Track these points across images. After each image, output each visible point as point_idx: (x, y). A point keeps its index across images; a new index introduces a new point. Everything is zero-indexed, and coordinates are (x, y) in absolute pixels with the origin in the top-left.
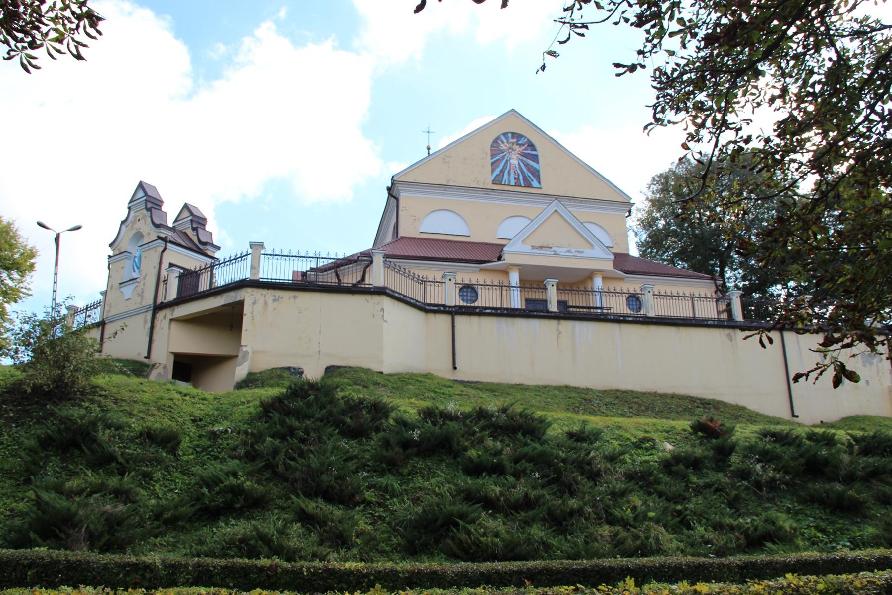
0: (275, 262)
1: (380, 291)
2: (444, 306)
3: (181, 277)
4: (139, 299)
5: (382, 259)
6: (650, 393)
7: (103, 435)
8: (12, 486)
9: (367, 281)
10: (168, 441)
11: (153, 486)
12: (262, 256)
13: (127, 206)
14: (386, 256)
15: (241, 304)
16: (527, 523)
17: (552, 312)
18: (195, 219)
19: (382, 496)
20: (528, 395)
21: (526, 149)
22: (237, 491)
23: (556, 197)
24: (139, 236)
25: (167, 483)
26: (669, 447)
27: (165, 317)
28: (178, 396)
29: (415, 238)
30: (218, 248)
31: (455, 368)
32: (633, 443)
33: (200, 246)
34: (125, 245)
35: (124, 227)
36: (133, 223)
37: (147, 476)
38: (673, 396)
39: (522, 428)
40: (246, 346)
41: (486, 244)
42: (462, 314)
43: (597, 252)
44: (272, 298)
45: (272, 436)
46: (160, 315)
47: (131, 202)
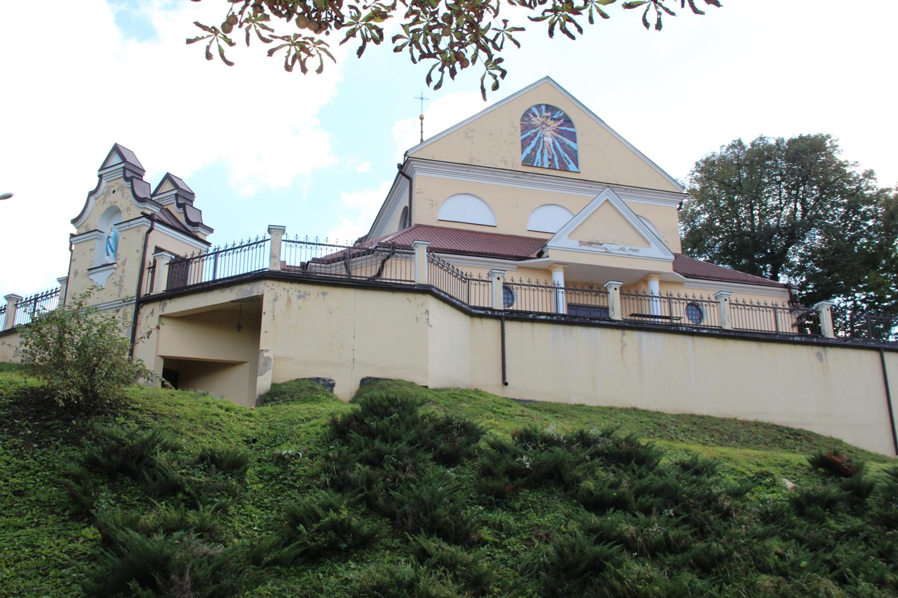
0: (298, 250)
1: (425, 290)
2: (491, 309)
3: (171, 264)
4: (116, 289)
5: (426, 253)
6: (729, 420)
7: (162, 458)
8: (56, 522)
9: (384, 276)
10: (233, 466)
11: (231, 522)
12: (283, 243)
13: (96, 173)
14: (430, 250)
15: (257, 301)
16: (678, 567)
17: (616, 321)
18: (181, 193)
19: (497, 534)
20: (594, 417)
21: (561, 125)
22: (341, 528)
23: (608, 185)
24: (114, 211)
25: (242, 518)
26: (789, 484)
27: (152, 313)
28: (222, 412)
29: (432, 227)
30: (211, 230)
31: (506, 384)
32: (750, 478)
33: (190, 228)
34: (94, 221)
35: (92, 199)
36: (106, 194)
37: (223, 508)
38: (757, 424)
39: (629, 457)
40: (267, 351)
41: (516, 237)
42: (512, 319)
43: (654, 251)
44: (297, 294)
45: (360, 462)
46: (146, 310)
47: (101, 169)
